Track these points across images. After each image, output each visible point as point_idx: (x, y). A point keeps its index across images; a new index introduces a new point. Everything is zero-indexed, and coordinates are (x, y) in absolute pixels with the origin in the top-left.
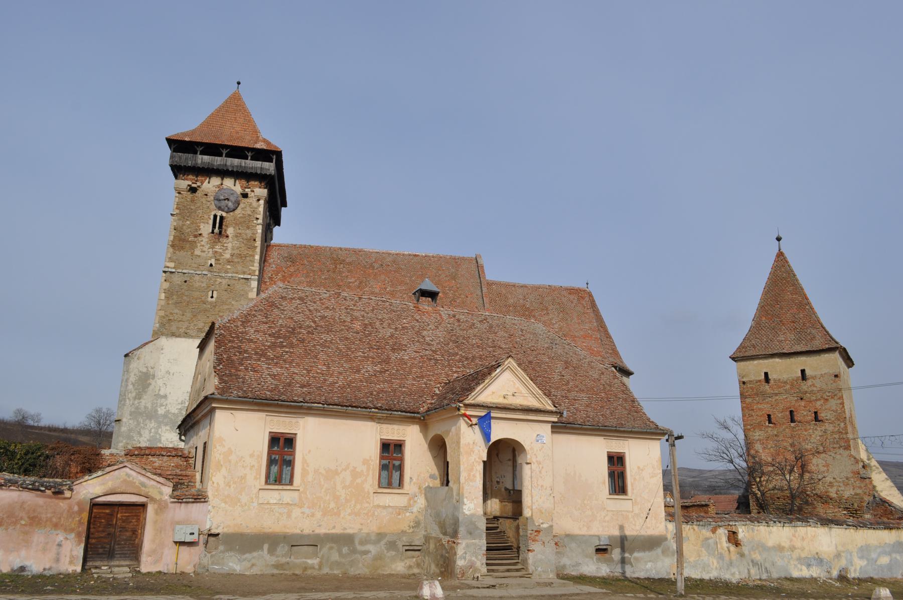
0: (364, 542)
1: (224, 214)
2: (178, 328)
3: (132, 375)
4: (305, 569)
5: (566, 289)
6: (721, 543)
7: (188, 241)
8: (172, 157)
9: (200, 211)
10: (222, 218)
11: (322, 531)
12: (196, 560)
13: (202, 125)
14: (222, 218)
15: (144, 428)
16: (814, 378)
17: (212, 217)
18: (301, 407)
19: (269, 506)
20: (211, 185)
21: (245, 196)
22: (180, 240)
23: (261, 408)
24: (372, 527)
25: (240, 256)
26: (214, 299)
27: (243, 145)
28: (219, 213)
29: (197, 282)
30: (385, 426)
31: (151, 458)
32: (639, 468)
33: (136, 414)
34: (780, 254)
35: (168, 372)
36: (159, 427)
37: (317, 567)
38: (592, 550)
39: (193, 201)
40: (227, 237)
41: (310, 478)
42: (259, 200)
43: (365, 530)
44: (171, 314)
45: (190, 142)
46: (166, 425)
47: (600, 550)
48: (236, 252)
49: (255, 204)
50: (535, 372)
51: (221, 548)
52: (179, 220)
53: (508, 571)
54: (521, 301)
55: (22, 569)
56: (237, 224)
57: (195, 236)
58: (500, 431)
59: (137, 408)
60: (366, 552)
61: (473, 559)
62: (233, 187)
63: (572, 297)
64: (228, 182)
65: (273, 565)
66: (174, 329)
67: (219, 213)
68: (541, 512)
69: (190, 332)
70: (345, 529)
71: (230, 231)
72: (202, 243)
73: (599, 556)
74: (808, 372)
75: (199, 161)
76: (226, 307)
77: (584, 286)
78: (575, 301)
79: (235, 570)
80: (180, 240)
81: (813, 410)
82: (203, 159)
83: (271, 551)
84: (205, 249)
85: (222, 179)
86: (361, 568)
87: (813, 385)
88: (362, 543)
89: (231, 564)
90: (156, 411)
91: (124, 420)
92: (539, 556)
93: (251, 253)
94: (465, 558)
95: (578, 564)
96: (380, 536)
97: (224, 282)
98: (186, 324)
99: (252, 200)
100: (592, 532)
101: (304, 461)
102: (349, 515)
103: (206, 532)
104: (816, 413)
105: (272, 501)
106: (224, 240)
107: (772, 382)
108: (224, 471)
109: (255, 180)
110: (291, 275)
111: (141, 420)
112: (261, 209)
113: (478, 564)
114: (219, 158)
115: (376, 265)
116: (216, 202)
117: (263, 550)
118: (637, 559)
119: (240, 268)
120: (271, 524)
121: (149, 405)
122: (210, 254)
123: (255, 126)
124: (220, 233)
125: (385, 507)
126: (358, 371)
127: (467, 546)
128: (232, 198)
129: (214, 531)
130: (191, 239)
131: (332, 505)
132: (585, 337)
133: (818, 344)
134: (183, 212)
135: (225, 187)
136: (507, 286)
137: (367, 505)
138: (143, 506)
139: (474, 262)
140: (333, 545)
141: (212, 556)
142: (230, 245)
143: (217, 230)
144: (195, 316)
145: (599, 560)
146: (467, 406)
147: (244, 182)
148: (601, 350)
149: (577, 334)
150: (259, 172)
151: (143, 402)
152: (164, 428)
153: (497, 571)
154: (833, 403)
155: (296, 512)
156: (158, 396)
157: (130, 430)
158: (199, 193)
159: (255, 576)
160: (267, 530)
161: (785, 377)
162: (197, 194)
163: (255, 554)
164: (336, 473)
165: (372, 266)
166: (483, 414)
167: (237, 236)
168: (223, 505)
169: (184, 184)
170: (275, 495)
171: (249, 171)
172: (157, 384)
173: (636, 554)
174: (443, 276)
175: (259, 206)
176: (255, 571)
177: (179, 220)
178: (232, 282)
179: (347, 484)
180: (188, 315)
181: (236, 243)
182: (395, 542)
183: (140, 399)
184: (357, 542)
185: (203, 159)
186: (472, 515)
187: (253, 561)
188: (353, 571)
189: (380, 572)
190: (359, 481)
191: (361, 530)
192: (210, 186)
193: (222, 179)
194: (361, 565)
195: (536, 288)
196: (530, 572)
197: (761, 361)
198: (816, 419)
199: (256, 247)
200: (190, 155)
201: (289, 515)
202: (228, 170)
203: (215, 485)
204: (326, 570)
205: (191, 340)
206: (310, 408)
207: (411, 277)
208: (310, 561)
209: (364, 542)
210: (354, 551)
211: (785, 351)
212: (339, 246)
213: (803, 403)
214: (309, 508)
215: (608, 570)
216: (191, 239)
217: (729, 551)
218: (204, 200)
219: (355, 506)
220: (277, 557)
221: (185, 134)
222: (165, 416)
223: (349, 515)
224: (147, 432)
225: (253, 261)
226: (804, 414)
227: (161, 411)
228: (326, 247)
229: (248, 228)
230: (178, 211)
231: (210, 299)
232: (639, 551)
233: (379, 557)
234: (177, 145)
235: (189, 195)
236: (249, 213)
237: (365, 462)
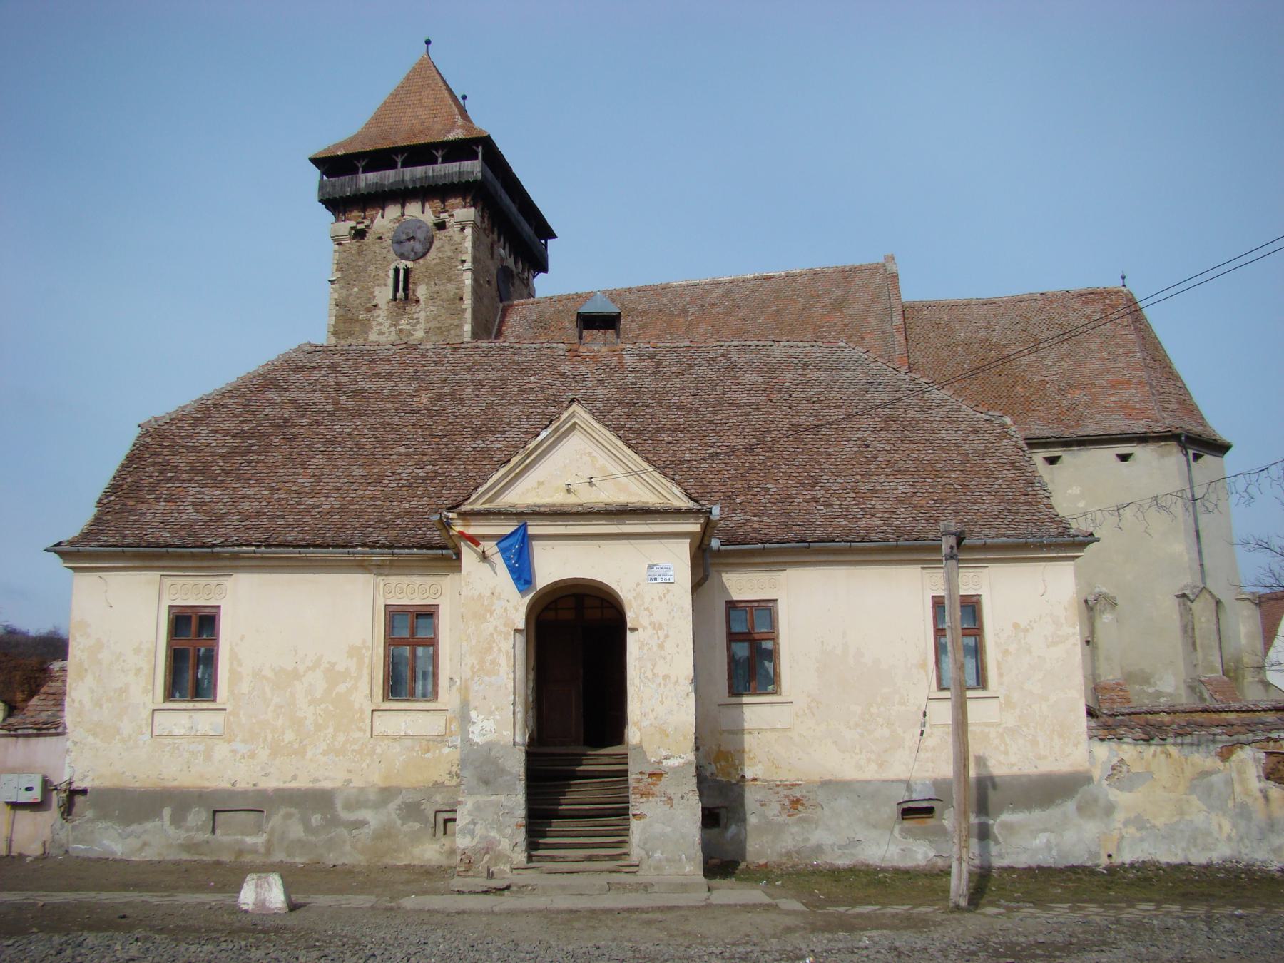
1: (410, 264)
4: (241, 853)
5: (1079, 295)
6: (1243, 781)
7: (358, 321)
8: (322, 187)
9: (372, 267)
10: (407, 271)
11: (271, 784)
12: (46, 834)
13: (368, 125)
14: (407, 271)
17: (391, 273)
18: (216, 556)
19: (170, 740)
20: (386, 221)
21: (441, 226)
23: (147, 564)
24: (371, 776)
27: (429, 139)
28: (402, 264)
30: (393, 580)
32: (1016, 626)
37: (262, 850)
38: (892, 811)
39: (360, 253)
41: (245, 687)
42: (463, 229)
43: (357, 783)
47: (909, 812)
48: (434, 324)
49: (457, 237)
50: (636, 427)
51: (89, 814)
52: (342, 288)
53: (590, 858)
54: (982, 332)
56: (432, 276)
57: (368, 311)
58: (556, 564)
60: (361, 824)
61: (493, 834)
63: (1089, 309)
64: (413, 209)
65: (181, 845)
67: (402, 264)
68: (664, 733)
70: (317, 780)
71: (421, 291)
72: (380, 320)
73: (909, 823)
75: (362, 184)
79: (113, 853)
83: (177, 820)
84: (385, 329)
85: (403, 206)
86: (349, 854)
88: (349, 806)
89: (106, 842)
92: (658, 828)
93: (456, 322)
94: (472, 834)
95: (854, 843)
96: (387, 794)
99: (452, 231)
100: (890, 775)
101: (233, 655)
102: (324, 753)
103: (64, 786)
105: (177, 731)
106: (412, 308)
108: (89, 679)
109: (456, 197)
112: (468, 244)
113: (505, 845)
114: (391, 173)
115: (691, 308)
117: (161, 818)
118: (1009, 827)
120: (177, 771)
125: (397, 738)
126: (379, 481)
127: (478, 808)
128: (420, 235)
129: (78, 785)
131: (289, 736)
132: (1114, 384)
134: (347, 274)
136: (953, 306)
137: (358, 734)
140: (292, 810)
141: (74, 828)
142: (422, 315)
143: (400, 294)
145: (906, 833)
146: (465, 516)
147: (437, 203)
148: (1149, 405)
149: (1097, 381)
150: (456, 180)
153: (563, 859)
155: (221, 750)
158: (370, 238)
162: (366, 240)
163: (149, 825)
164: (296, 675)
165: (684, 311)
166: (509, 530)
168: (91, 739)
169: (345, 227)
170: (186, 720)
173: (1006, 817)
174: (819, 306)
175: (464, 238)
176: (149, 854)
177: (342, 288)
179: (318, 695)
181: (433, 310)
182: (418, 804)
184: (339, 805)
185: (389, 177)
186: (490, 746)
187: (145, 837)
188: (331, 858)
189: (388, 861)
190: (342, 688)
191: (350, 781)
192: (385, 221)
193: (443, 202)
194: (348, 847)
195: (1015, 302)
196: (634, 859)
201: (208, 757)
202: (407, 188)
203: (77, 705)
206: (235, 556)
207: (755, 319)
208: (249, 840)
209: (351, 805)
210: (334, 822)
212: (626, 286)
214: (243, 741)
215: (931, 854)
217: (1266, 798)
218: (377, 248)
219: (334, 737)
220: (188, 830)
221: (338, 146)
223: (324, 753)
229: (449, 280)
230: (339, 275)
232: (1014, 810)
233: (385, 833)
234: (331, 165)
235: (354, 244)
236: (450, 254)
237: (353, 652)
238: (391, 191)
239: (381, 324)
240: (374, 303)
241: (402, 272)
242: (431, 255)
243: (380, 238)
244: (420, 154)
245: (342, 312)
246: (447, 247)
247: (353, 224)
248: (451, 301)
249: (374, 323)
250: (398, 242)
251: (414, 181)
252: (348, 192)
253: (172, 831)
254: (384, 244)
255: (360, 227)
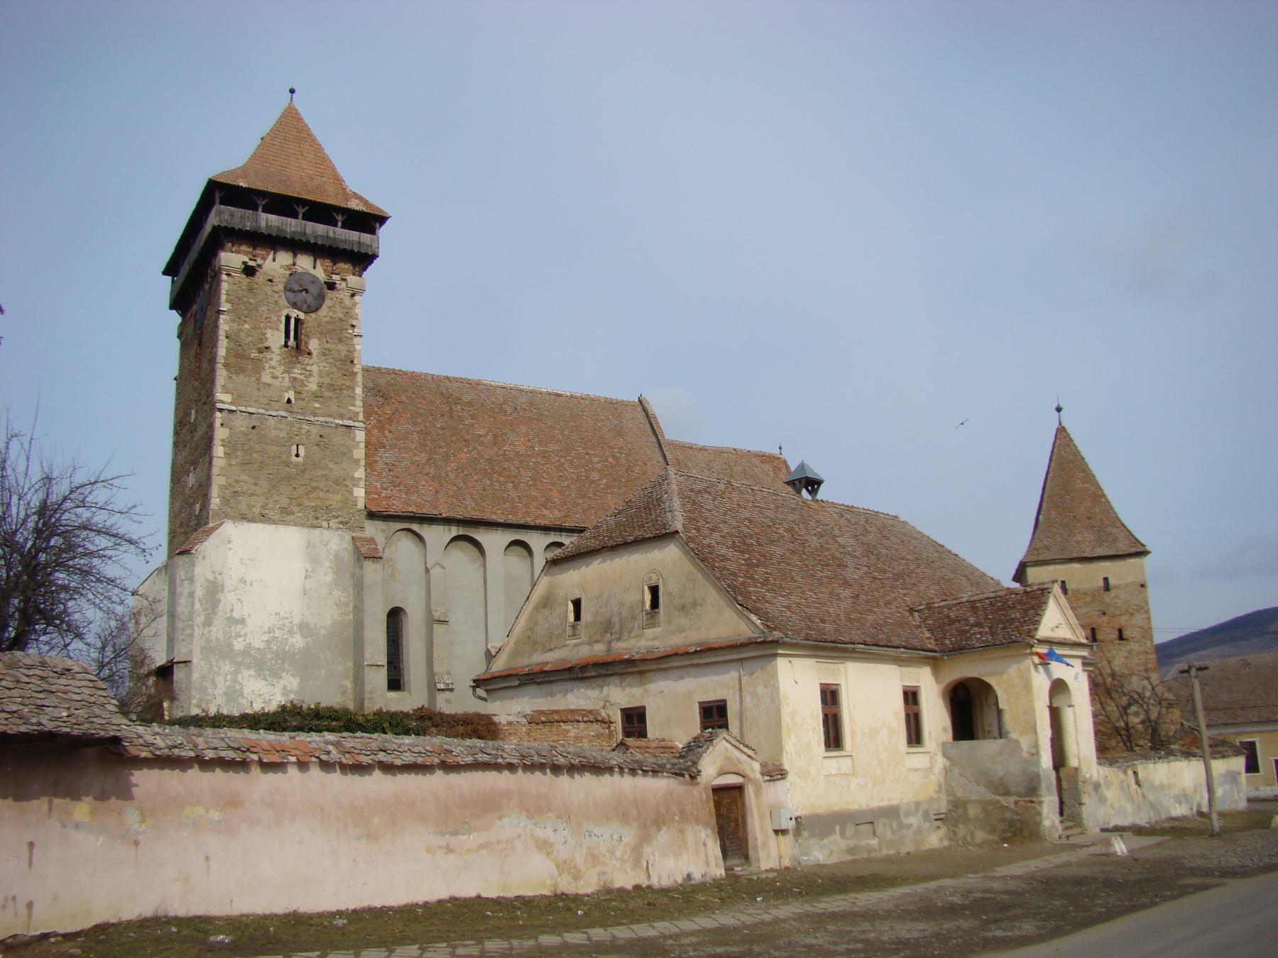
0: (907, 814)
1: (302, 316)
2: (250, 507)
3: (198, 585)
7: (249, 358)
9: (264, 308)
10: (297, 320)
13: (254, 157)
14: (297, 320)
15: (218, 674)
16: (1118, 587)
17: (283, 319)
20: (277, 264)
21: (331, 286)
22: (237, 356)
25: (332, 387)
26: (300, 459)
28: (294, 313)
29: (274, 430)
31: (563, 726)
33: (207, 650)
34: (1061, 431)
35: (243, 581)
36: (237, 671)
39: (251, 289)
40: (310, 354)
44: (237, 481)
45: (249, 190)
46: (248, 668)
48: (327, 380)
55: (689, 877)
57: (260, 351)
59: (208, 641)
62: (312, 271)
63: (767, 467)
66: (243, 507)
69: (270, 514)
71: (314, 345)
74: (1112, 581)
76: (320, 473)
77: (776, 452)
78: (771, 473)
80: (237, 356)
81: (1117, 626)
82: (269, 221)
84: (278, 374)
85: (295, 256)
87: (1117, 597)
90: (230, 645)
91: (195, 661)
93: (348, 383)
97: (315, 430)
98: (261, 500)
104: (1120, 631)
107: (1070, 593)
110: (390, 420)
111: (213, 661)
116: (290, 295)
119: (334, 408)
121: (221, 636)
122: (287, 383)
123: (334, 169)
124: (298, 347)
130: (254, 354)
133: (1122, 547)
135: (300, 270)
138: (739, 788)
139: (640, 409)
142: (315, 369)
143: (292, 342)
144: (274, 486)
147: (328, 263)
151: (214, 629)
152: (246, 673)
154: (1139, 619)
155: (854, 783)
156: (232, 621)
157: (203, 678)
158: (260, 278)
159: (836, 865)
160: (836, 808)
161: (1086, 586)
162: (256, 279)
167: (325, 353)
171: (342, 246)
172: (228, 598)
178: (325, 432)
180: (265, 485)
183: (210, 625)
185: (269, 221)
192: (276, 265)
193: (295, 256)
197: (1057, 567)
198: (1121, 637)
199: (355, 374)
200: (249, 212)
202: (308, 242)
204: (885, 852)
205: (273, 527)
211: (1087, 555)
213: (1105, 619)
216: (254, 354)
218: (268, 289)
222: (246, 653)
224: (221, 679)
225: (353, 398)
226: (1108, 634)
227: (238, 645)
228: (426, 374)
229: (340, 340)
231: (294, 459)
233: (919, 831)
235: (246, 280)
236: (341, 316)
238: (292, 239)
239: (274, 368)
240: (267, 344)
241: (293, 321)
242: (323, 312)
243: (270, 281)
244: (283, 205)
245: (232, 346)
246: (338, 308)
247: (246, 259)
248: (343, 361)
249: (267, 365)
250: (288, 289)
251: (316, 237)
252: (248, 226)
253: (840, 841)
254: (276, 289)
255: (252, 263)
